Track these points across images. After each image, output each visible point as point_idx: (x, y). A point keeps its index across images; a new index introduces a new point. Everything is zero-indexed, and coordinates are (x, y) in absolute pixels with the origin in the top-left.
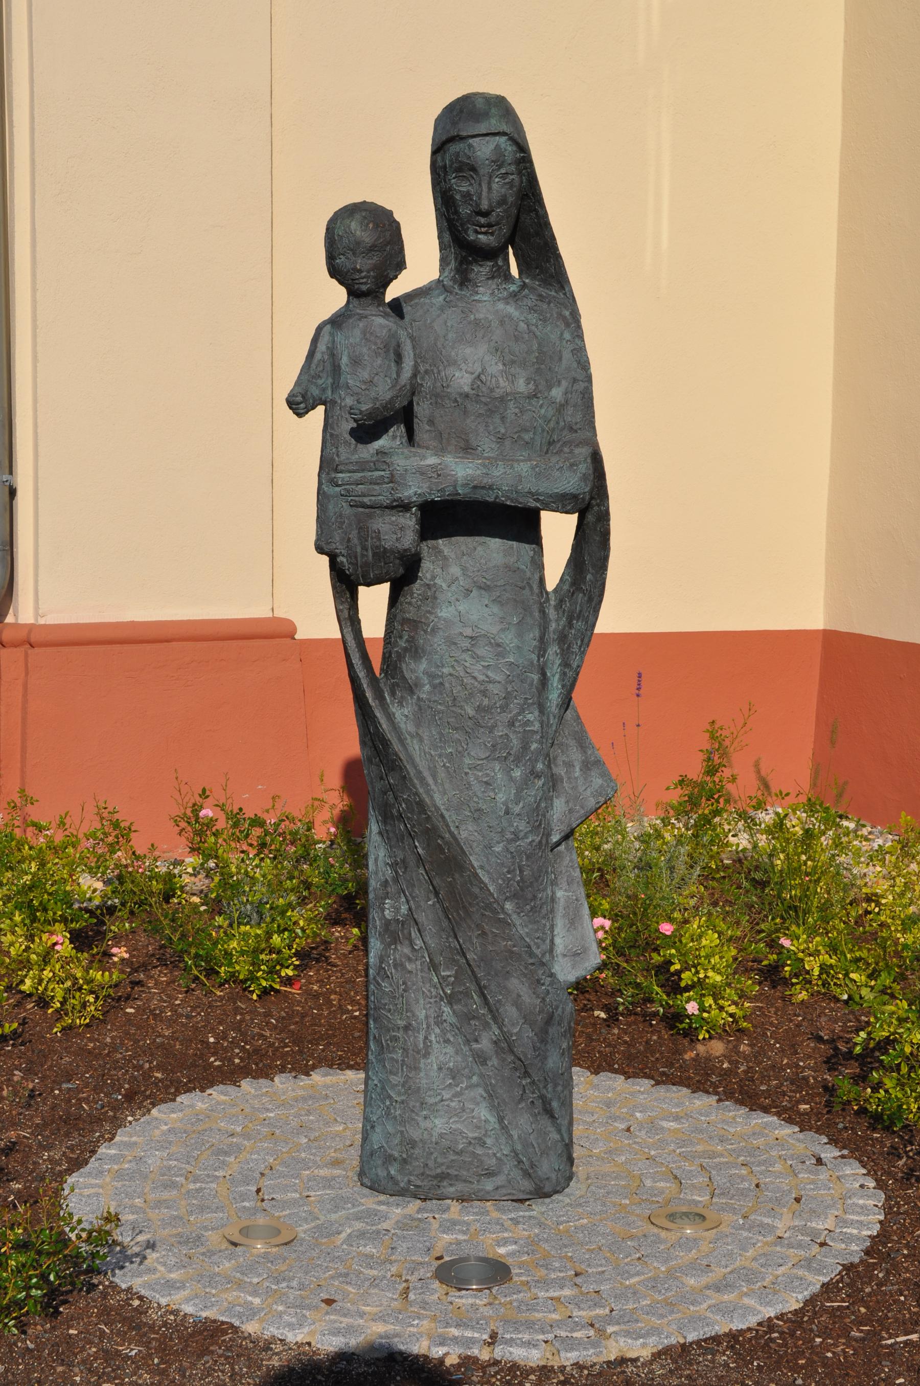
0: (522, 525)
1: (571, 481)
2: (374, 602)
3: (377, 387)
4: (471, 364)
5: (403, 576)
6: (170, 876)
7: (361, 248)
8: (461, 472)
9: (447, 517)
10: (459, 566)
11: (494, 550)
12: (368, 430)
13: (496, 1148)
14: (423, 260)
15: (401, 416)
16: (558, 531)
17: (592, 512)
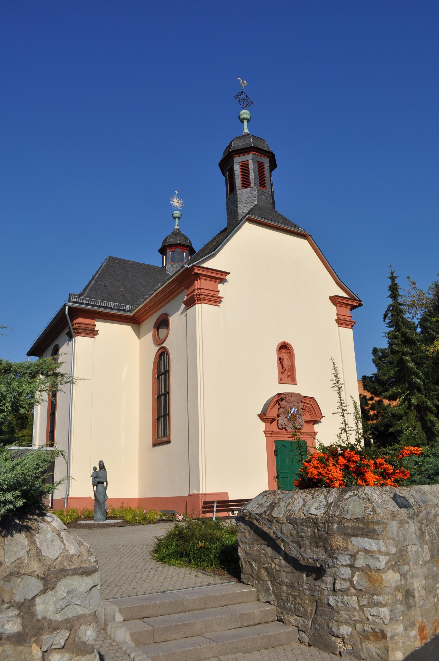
0: (103, 483)
1: (105, 480)
2: (95, 487)
3: (95, 476)
4: (100, 474)
5: (97, 486)
6: (17, 480)
7: (95, 469)
8: (99, 480)
9: (99, 483)
10: (100, 485)
11: (101, 484)
12: (95, 478)
13: (101, 518)
14: (98, 469)
15: (97, 477)
16: (105, 483)
17: (107, 481)
